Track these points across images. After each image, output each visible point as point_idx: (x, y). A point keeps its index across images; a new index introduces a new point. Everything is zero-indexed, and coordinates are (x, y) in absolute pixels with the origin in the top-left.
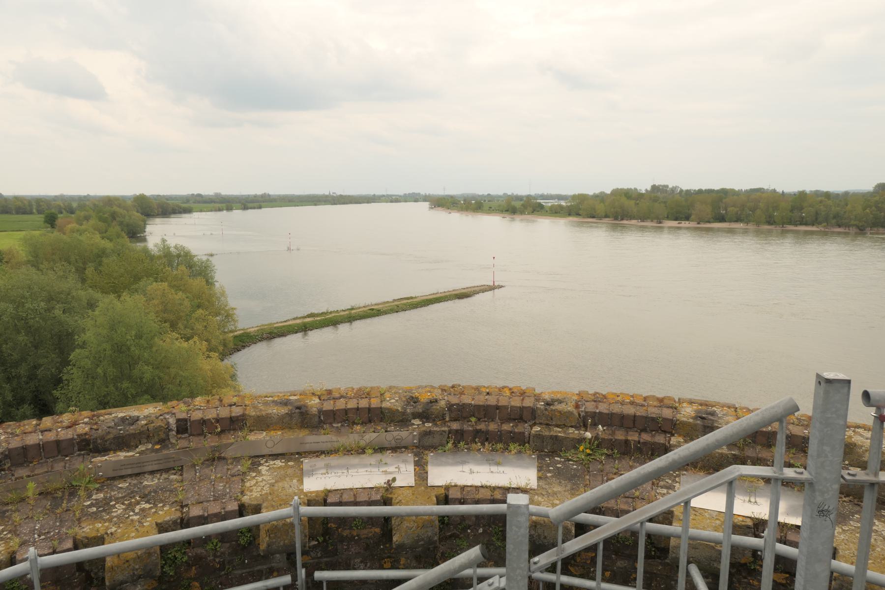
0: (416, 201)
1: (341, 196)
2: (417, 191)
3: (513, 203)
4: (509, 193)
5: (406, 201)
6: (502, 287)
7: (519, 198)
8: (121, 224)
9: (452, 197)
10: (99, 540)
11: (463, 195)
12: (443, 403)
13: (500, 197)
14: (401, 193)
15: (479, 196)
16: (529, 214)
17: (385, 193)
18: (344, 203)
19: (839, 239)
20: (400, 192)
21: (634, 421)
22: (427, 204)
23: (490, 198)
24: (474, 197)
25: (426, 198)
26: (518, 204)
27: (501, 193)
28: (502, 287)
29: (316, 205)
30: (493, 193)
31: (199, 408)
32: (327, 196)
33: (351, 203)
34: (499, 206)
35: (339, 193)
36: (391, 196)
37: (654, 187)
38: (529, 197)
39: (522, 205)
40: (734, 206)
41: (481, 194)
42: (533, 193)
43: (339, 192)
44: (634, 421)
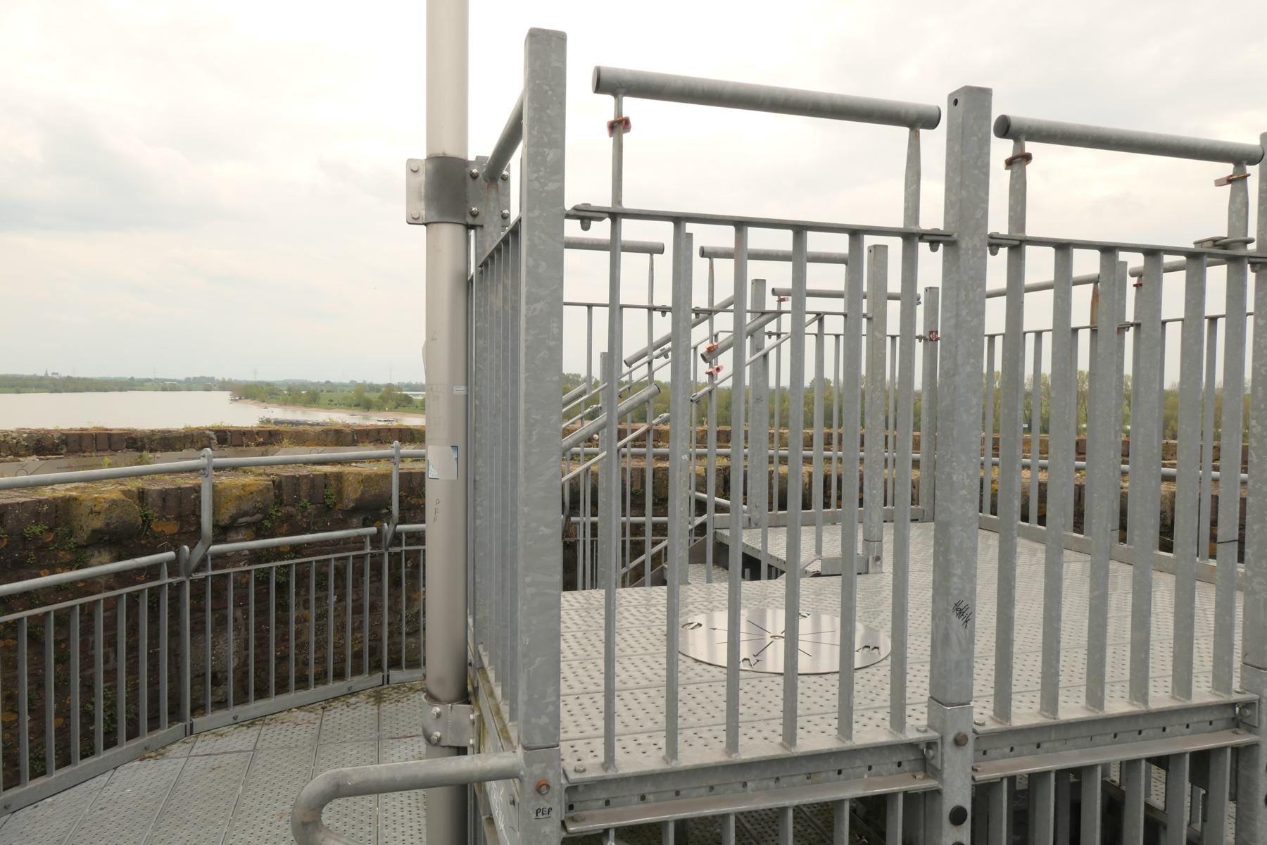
0: (208, 389)
1: (69, 378)
3: (366, 395)
5: (190, 390)
7: (374, 388)
9: (268, 384)
10: (917, 415)
11: (285, 383)
14: (182, 377)
16: (390, 410)
17: (151, 377)
18: (106, 391)
19: (490, 771)
22: (226, 395)
23: (330, 387)
24: (304, 385)
25: (223, 386)
26: (374, 396)
27: (347, 381)
29: (18, 392)
30: (335, 379)
31: (924, 404)
32: (41, 378)
33: (88, 390)
34: (345, 398)
35: (64, 374)
36: (163, 381)
37: (328, 382)
38: (389, 386)
39: (381, 397)
40: (168, 520)
41: (315, 381)
42: (395, 382)
43: (127, 375)
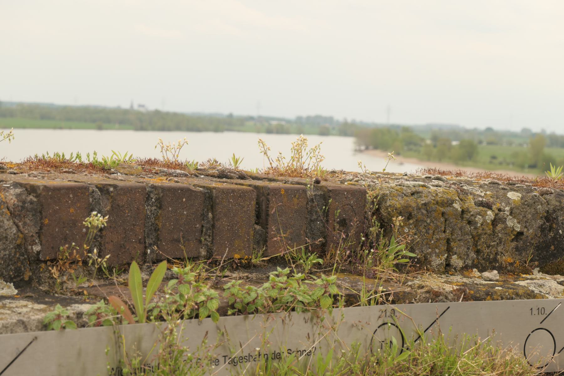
2: (325, 113)
3: (547, 151)
4: (536, 129)
6: (234, 155)
8: (86, 315)
9: (406, 129)
12: (189, 267)
13: (514, 135)
15: (467, 131)
17: (254, 113)
20: (290, 113)
21: (261, 217)
24: (455, 133)
27: (516, 128)
28: (234, 155)
30: (499, 126)
32: (126, 112)
34: (515, 155)
36: (268, 119)
43: (153, 103)
44: (261, 217)
